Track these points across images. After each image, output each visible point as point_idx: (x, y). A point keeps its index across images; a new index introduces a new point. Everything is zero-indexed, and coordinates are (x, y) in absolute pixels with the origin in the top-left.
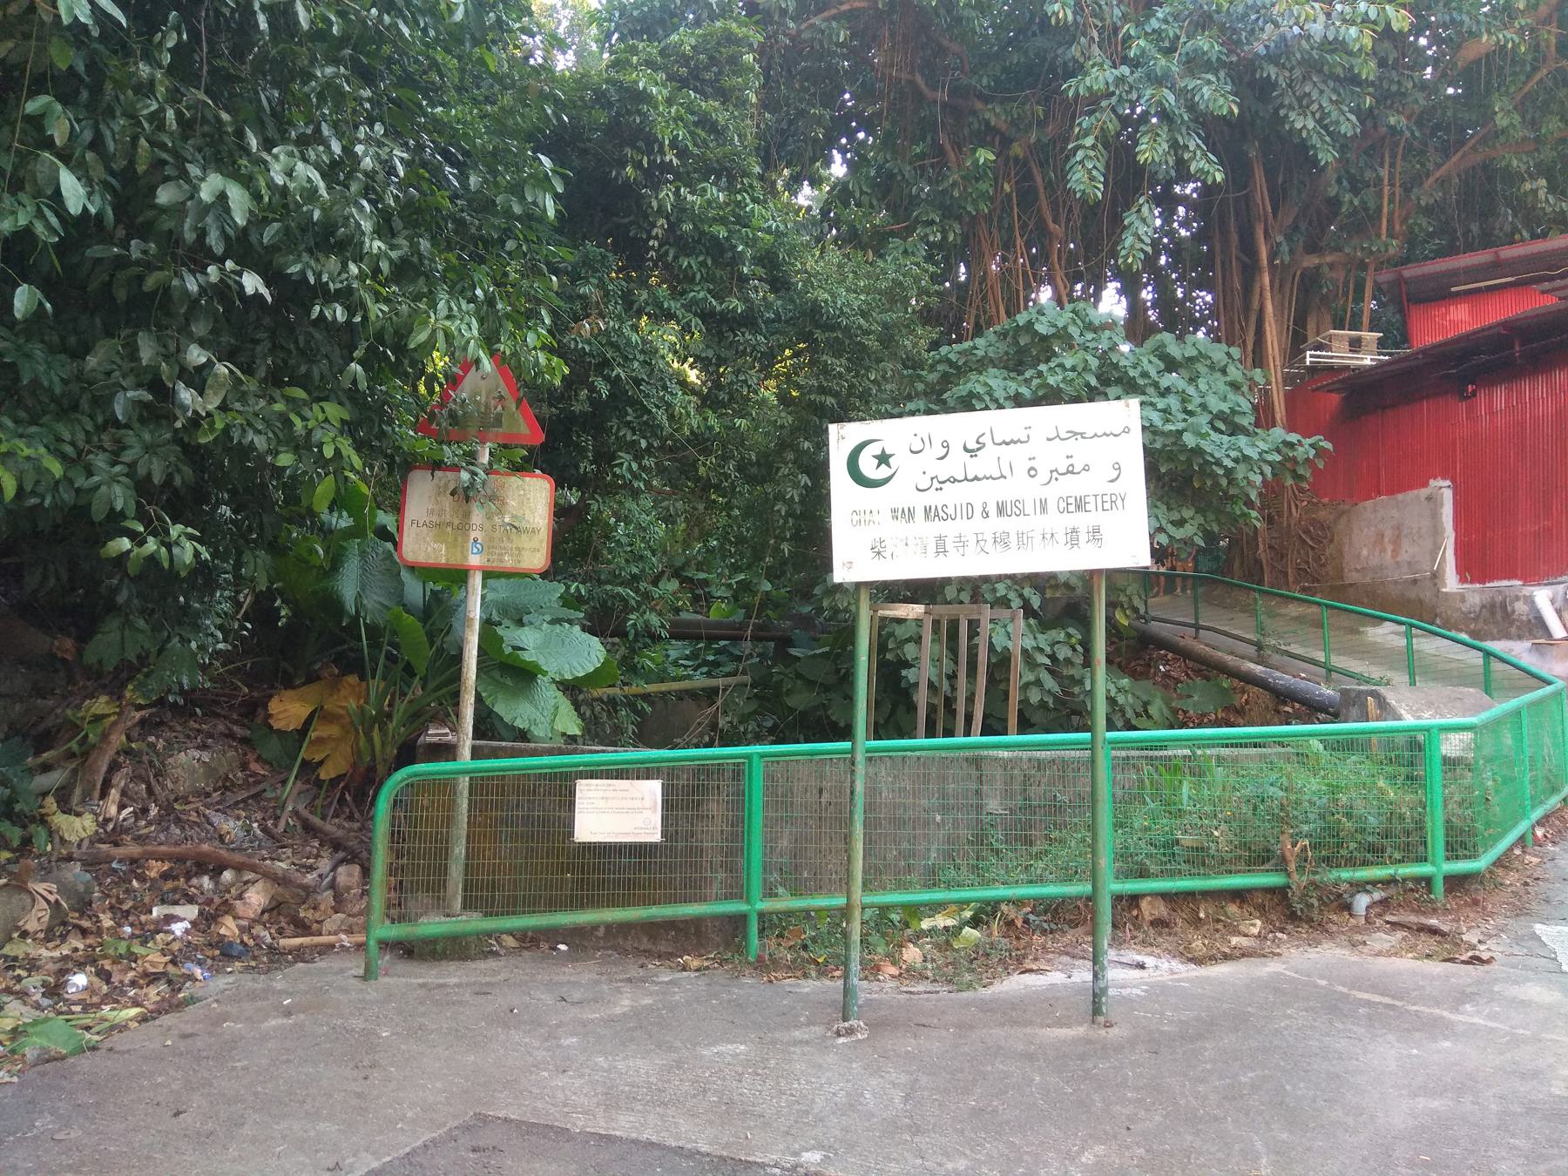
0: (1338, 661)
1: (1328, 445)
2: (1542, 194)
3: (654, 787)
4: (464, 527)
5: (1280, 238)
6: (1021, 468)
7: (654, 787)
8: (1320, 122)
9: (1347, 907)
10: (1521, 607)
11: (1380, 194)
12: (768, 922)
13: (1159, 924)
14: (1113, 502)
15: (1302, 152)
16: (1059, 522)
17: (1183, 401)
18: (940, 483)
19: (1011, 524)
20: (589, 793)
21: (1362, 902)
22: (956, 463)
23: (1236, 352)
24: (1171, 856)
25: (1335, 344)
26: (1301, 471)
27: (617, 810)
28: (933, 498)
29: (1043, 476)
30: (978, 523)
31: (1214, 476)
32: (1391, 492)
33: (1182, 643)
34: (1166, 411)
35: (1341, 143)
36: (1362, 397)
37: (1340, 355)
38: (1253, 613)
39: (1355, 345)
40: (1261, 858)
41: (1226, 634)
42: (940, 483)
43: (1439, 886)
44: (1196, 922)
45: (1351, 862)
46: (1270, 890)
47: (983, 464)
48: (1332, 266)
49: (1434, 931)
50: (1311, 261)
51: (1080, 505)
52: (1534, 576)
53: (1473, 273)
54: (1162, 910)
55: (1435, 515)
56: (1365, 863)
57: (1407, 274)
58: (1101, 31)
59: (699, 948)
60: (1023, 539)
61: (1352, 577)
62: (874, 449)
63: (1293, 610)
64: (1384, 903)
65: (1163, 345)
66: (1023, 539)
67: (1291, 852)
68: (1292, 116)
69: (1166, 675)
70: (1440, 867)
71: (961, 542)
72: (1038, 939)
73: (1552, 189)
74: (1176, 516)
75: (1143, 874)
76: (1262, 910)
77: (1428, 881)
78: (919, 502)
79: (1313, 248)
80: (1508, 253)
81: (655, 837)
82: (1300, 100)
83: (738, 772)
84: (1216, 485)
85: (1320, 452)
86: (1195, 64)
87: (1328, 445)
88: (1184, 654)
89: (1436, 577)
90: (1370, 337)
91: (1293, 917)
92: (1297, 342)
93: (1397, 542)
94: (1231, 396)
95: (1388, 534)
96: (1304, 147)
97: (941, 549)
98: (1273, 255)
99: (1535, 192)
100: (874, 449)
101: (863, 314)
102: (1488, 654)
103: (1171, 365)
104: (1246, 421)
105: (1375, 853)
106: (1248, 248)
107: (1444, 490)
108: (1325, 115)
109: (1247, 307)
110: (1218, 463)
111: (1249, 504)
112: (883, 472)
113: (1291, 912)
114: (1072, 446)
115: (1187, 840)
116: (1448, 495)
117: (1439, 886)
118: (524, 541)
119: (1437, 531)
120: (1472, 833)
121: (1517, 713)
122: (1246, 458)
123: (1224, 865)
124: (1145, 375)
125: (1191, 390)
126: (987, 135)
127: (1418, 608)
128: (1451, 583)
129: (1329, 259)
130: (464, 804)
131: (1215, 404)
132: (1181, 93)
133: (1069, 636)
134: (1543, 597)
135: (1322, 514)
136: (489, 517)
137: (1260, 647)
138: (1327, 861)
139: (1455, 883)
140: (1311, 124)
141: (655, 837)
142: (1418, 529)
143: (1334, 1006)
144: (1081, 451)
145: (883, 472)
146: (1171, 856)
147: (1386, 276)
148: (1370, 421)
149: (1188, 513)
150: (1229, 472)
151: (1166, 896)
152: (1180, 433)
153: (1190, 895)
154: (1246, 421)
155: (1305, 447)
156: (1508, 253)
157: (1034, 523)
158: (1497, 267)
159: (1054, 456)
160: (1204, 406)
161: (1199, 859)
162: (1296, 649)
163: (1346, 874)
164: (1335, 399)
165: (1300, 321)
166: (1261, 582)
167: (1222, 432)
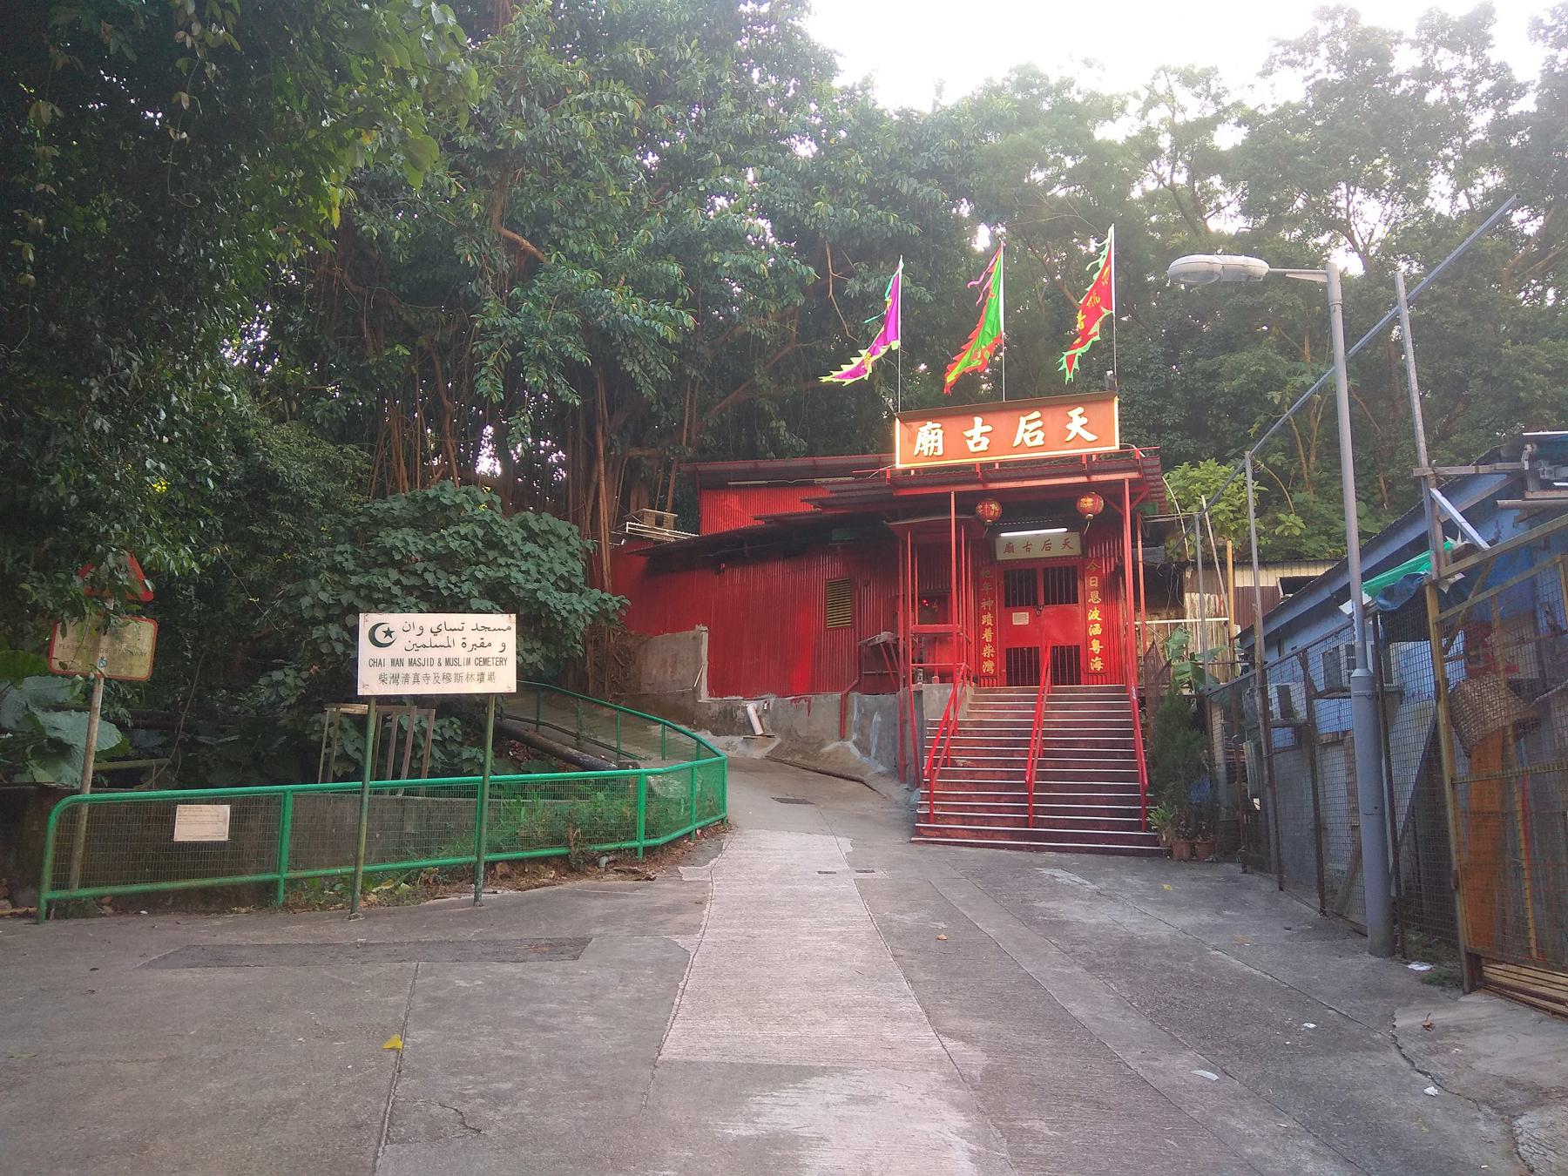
0: (624, 747)
1: (626, 601)
2: (782, 431)
3: (227, 808)
4: (95, 650)
5: (615, 437)
6: (459, 642)
7: (227, 808)
8: (646, 373)
9: (597, 864)
10: (740, 713)
11: (683, 412)
12: (291, 883)
13: (505, 877)
14: (502, 661)
15: (629, 382)
16: (474, 670)
17: (538, 565)
18: (417, 647)
19: (452, 670)
20: (184, 813)
21: (605, 860)
22: (426, 638)
23: (575, 528)
24: (514, 842)
25: (646, 518)
26: (612, 616)
27: (202, 822)
28: (413, 655)
29: (469, 647)
30: (435, 668)
31: (554, 620)
32: (673, 631)
33: (527, 734)
34: (527, 572)
35: (658, 383)
36: (662, 559)
37: (647, 528)
38: (576, 712)
39: (659, 522)
40: (558, 840)
41: (556, 727)
42: (417, 647)
43: (640, 851)
44: (523, 874)
45: (600, 841)
46: (559, 856)
47: (440, 639)
48: (648, 457)
49: (634, 872)
50: (635, 452)
51: (486, 661)
52: (749, 696)
53: (746, 475)
54: (506, 869)
55: (698, 651)
56: (608, 842)
57: (700, 468)
58: (495, 278)
59: (240, 902)
60: (458, 677)
61: (646, 689)
62: (384, 628)
63: (606, 712)
64: (615, 861)
65: (526, 520)
66: (458, 677)
67: (572, 835)
68: (625, 361)
69: (513, 758)
70: (642, 843)
71: (427, 677)
72: (441, 887)
73: (788, 429)
74: (529, 646)
75: (500, 850)
76: (555, 867)
77: (636, 849)
78: (406, 656)
79: (637, 442)
80: (763, 464)
81: (226, 838)
82: (631, 350)
83: (275, 802)
84: (555, 627)
85: (623, 606)
86: (566, 327)
87: (626, 601)
88: (528, 743)
89: (696, 691)
90: (669, 516)
91: (571, 870)
92: (619, 521)
93: (674, 666)
94: (570, 562)
95: (669, 660)
96: (633, 382)
97: (416, 680)
98: (608, 450)
99: (778, 428)
100: (384, 628)
101: (310, 483)
102: (699, 742)
103: (532, 536)
104: (578, 581)
105: (611, 837)
106: (591, 435)
107: (703, 632)
108: (647, 364)
109: (588, 480)
110: (559, 613)
111: (577, 642)
112: (388, 640)
113: (569, 866)
114: (483, 634)
115: (522, 833)
116: (705, 636)
117: (640, 851)
118: (135, 661)
119: (698, 661)
120: (657, 825)
121: (692, 768)
122: (576, 611)
123: (539, 845)
124: (513, 543)
125: (544, 556)
126: (409, 335)
127: (682, 713)
128: (704, 697)
129: (647, 453)
130: (84, 822)
131: (561, 570)
132: (554, 344)
133: (452, 723)
134: (751, 708)
135: (630, 643)
136: (112, 644)
137: (577, 736)
138: (590, 841)
139: (649, 850)
140: (637, 370)
141: (226, 838)
142: (685, 658)
143: (582, 895)
144: (488, 637)
145: (388, 640)
146: (514, 842)
147: (685, 468)
148: (660, 583)
149: (537, 645)
150: (564, 619)
151: (508, 861)
152: (535, 591)
153: (521, 861)
154: (578, 581)
155: (614, 602)
156: (763, 464)
157: (465, 670)
158: (756, 473)
159: (474, 638)
160: (551, 570)
161: (528, 843)
162: (601, 739)
163: (597, 847)
164: (642, 562)
165: (625, 503)
166: (585, 692)
167: (562, 590)
